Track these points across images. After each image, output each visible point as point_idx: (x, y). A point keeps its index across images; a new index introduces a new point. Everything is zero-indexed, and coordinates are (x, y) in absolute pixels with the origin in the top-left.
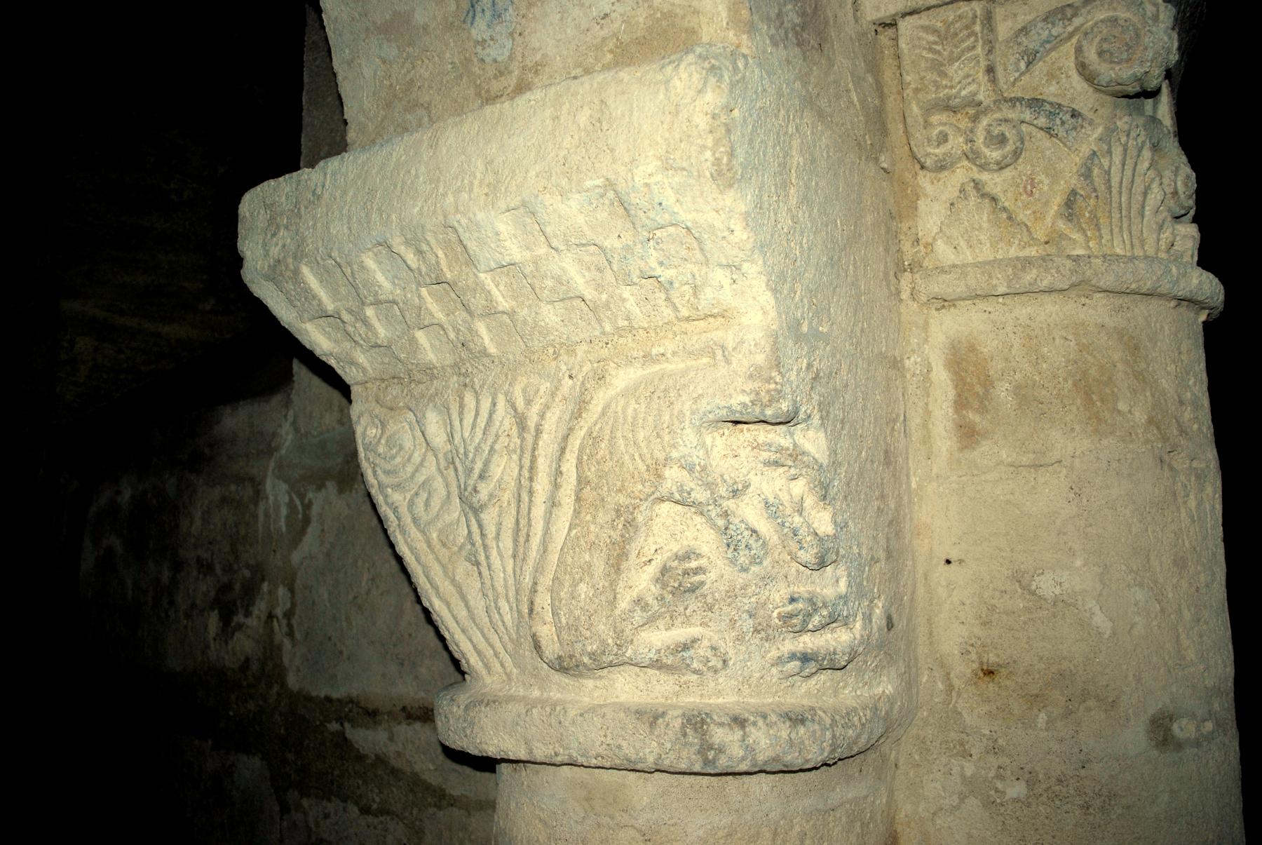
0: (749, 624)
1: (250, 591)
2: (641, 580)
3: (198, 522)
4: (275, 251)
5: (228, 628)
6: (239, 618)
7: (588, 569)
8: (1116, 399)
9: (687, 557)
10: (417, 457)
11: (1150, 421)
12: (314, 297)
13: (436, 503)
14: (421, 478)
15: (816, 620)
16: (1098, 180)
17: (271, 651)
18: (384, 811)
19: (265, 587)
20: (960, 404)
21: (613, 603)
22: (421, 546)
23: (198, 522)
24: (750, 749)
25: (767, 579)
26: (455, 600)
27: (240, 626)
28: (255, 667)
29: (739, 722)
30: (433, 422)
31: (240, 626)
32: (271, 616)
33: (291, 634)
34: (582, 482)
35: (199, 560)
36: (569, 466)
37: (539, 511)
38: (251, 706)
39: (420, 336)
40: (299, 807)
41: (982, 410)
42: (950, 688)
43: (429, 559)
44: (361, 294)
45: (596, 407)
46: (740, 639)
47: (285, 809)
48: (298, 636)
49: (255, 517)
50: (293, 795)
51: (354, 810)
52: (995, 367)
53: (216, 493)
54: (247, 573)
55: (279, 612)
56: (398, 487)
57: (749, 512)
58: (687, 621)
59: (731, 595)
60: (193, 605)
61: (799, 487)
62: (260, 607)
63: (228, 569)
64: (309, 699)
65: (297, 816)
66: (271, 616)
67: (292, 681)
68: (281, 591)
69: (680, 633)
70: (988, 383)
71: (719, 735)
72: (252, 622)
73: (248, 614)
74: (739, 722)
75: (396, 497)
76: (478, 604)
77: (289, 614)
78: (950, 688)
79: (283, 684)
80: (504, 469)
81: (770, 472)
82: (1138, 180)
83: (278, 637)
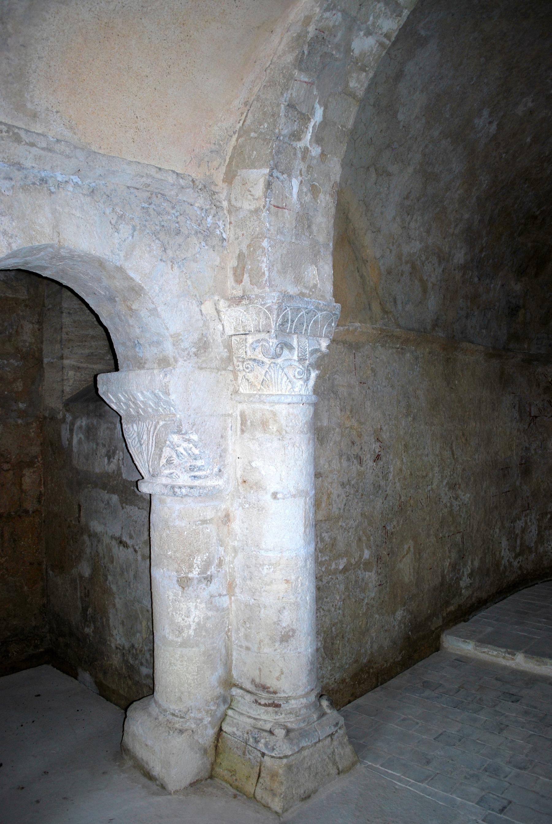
0: (183, 470)
1: (114, 453)
2: (163, 461)
3: (102, 433)
4: (104, 389)
5: (109, 462)
6: (112, 459)
7: (156, 458)
8: (269, 425)
9: (170, 457)
10: (133, 433)
11: (277, 430)
12: (307, 128)
13: (136, 443)
14: (133, 437)
15: (196, 470)
16: (269, 377)
17: (119, 469)
18: (143, 509)
19: (117, 452)
20: (242, 424)
21: (159, 465)
22: (133, 451)
23: (102, 433)
24: (182, 493)
25: (186, 462)
26: (139, 462)
27: (112, 462)
28: (116, 472)
29: (180, 488)
30: (135, 426)
31: (112, 462)
32: (119, 460)
33: (123, 464)
34: (156, 442)
35: (102, 443)
36: (154, 439)
37: (150, 447)
38: (115, 482)
39: (131, 409)
40: (126, 508)
41: (245, 426)
42: (238, 484)
43: (135, 454)
44: (119, 400)
45: (158, 427)
46: (182, 473)
47: (123, 508)
48: (125, 465)
49: (115, 433)
50: (124, 505)
51: (137, 508)
52: (248, 417)
53: (106, 425)
54: (113, 448)
55: (121, 459)
56: (129, 438)
57: (181, 450)
58: (173, 469)
59: (180, 465)
60: (101, 455)
61: (191, 445)
62: (116, 457)
63: (109, 446)
64: (127, 481)
65: (125, 510)
66: (119, 460)
67: (124, 476)
68: (121, 453)
69: (171, 471)
70: (246, 421)
71: (176, 490)
72: (115, 461)
73: (114, 459)
74: (180, 488)
75: (129, 440)
76: (143, 463)
77: (123, 459)
78: (238, 484)
79: (122, 477)
80: (145, 437)
81: (185, 443)
82: (279, 376)
83: (121, 465)
